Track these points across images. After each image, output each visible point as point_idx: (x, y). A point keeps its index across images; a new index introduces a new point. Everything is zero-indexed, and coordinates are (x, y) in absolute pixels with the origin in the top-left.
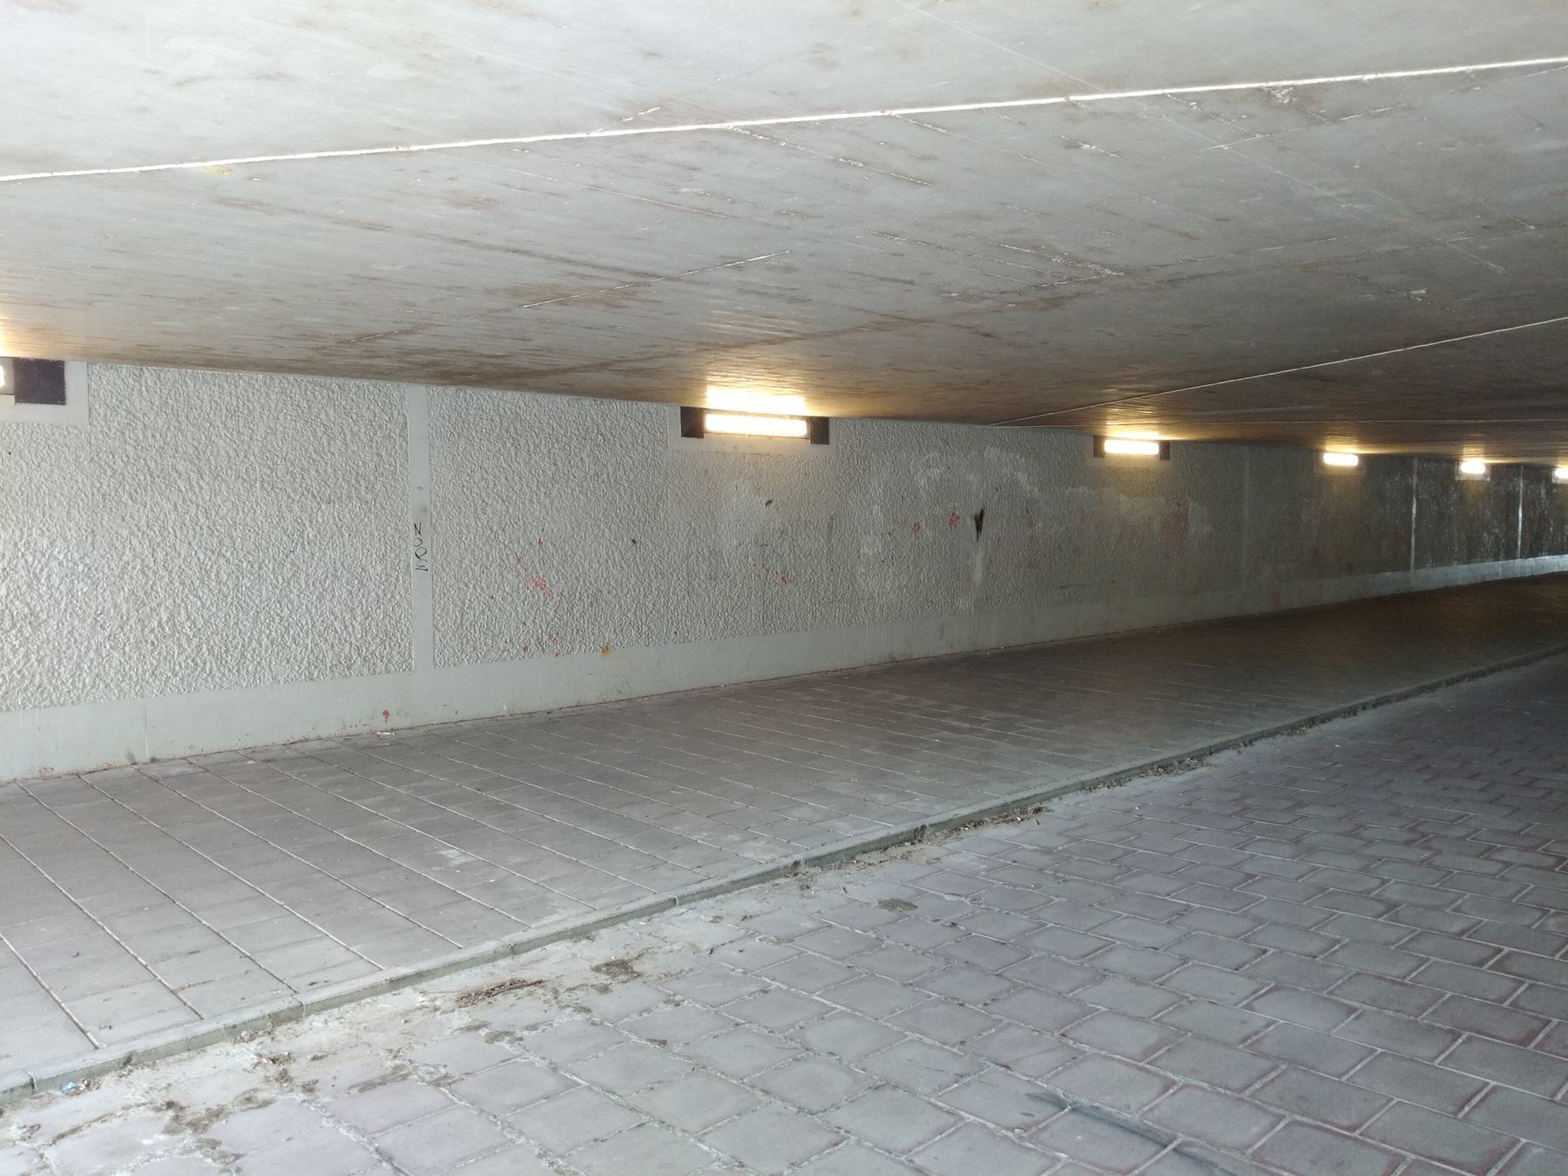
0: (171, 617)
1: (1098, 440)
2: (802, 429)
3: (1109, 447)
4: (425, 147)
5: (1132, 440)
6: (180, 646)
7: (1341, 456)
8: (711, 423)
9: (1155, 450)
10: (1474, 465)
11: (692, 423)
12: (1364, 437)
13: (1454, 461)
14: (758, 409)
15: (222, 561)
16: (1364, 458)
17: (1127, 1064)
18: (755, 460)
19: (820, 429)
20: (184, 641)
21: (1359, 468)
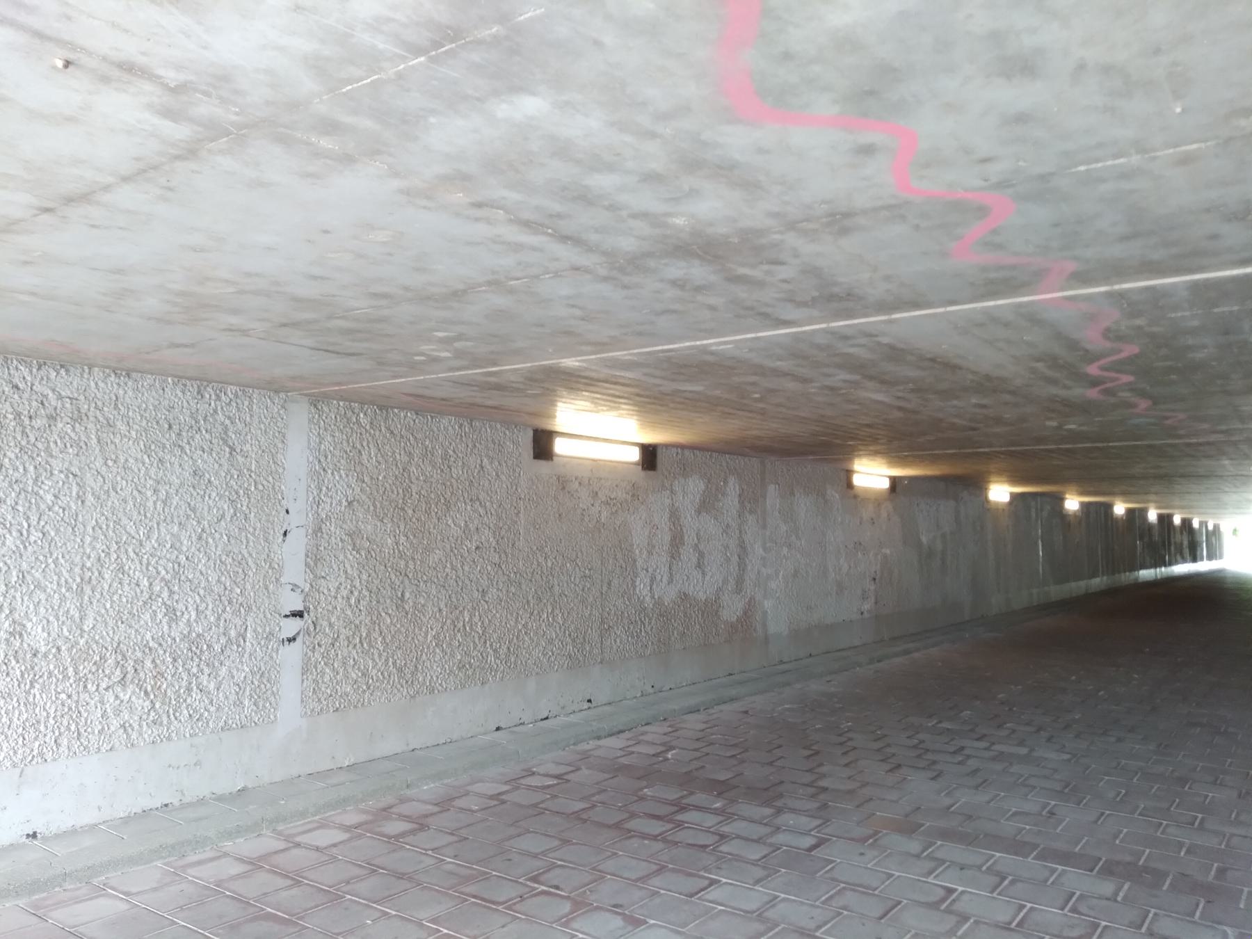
0: (369, 634)
1: (849, 473)
2: (634, 455)
3: (858, 480)
4: (1110, 163)
5: (872, 474)
6: (373, 660)
7: (1000, 492)
8: (560, 447)
9: (885, 484)
10: (1072, 503)
11: (542, 444)
12: (1015, 479)
13: (1060, 499)
14: (599, 434)
15: (407, 581)
16: (1082, 504)
17: (672, 930)
18: (594, 478)
19: (650, 455)
20: (376, 656)
21: (1010, 503)
